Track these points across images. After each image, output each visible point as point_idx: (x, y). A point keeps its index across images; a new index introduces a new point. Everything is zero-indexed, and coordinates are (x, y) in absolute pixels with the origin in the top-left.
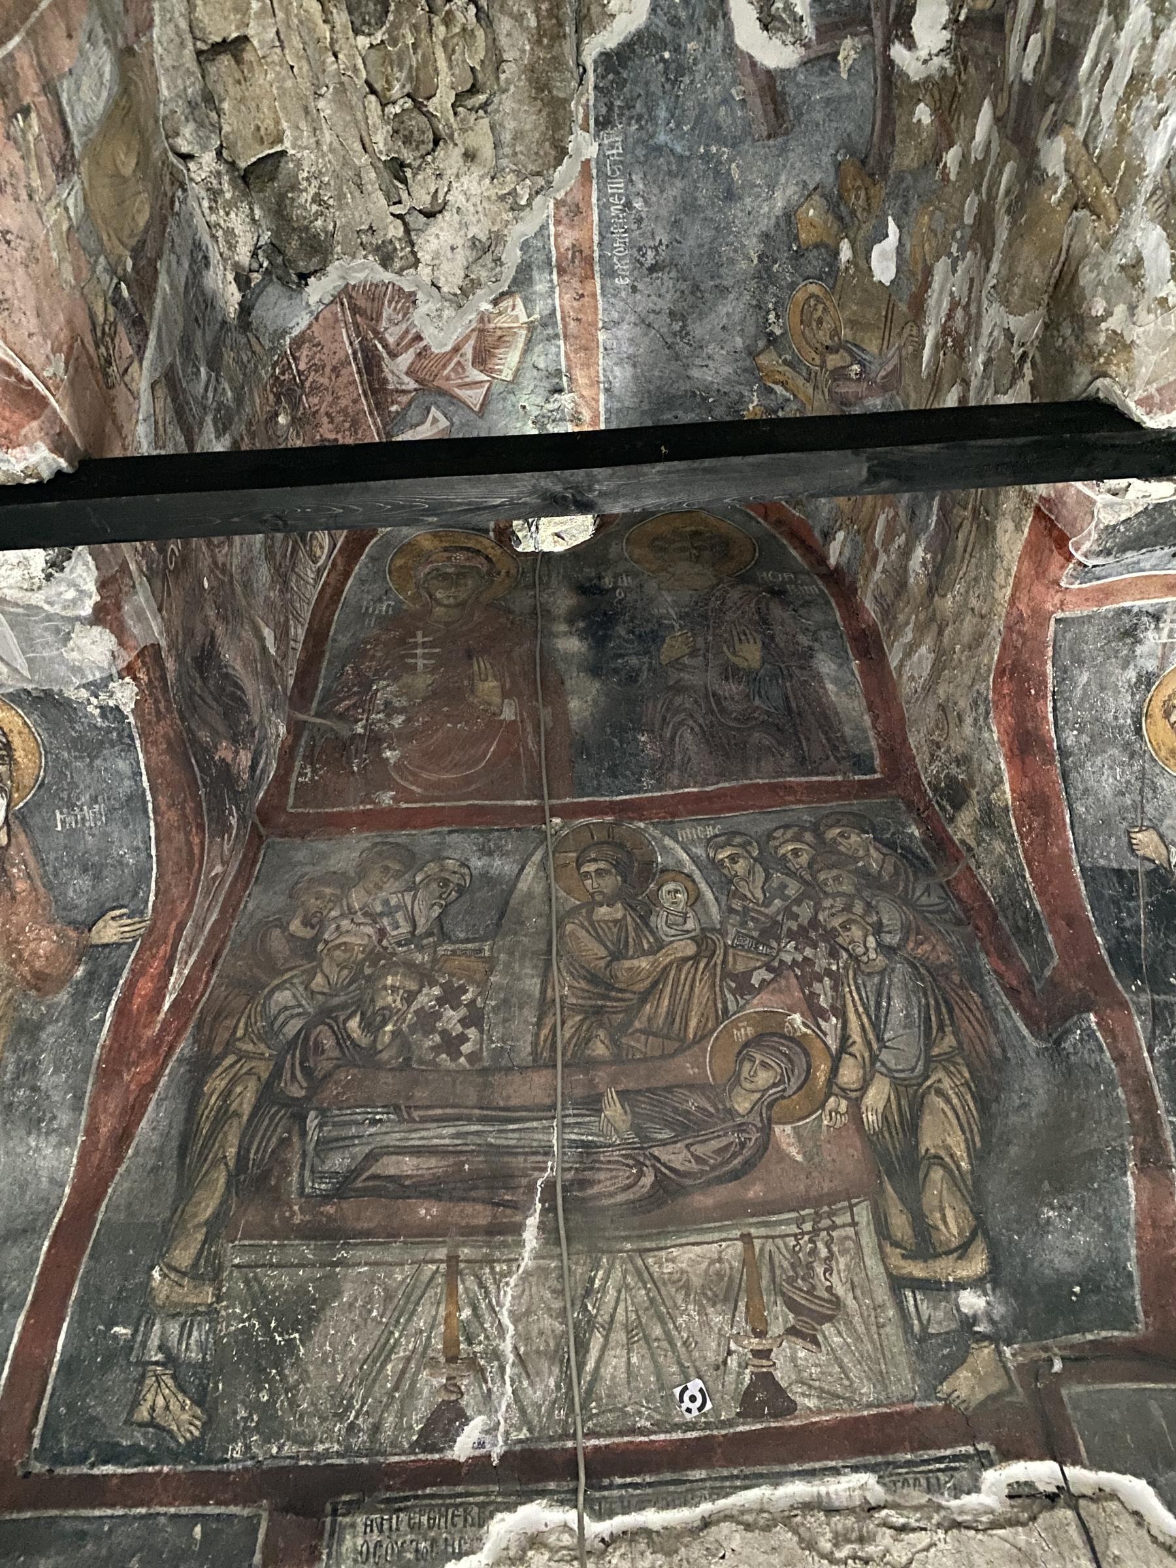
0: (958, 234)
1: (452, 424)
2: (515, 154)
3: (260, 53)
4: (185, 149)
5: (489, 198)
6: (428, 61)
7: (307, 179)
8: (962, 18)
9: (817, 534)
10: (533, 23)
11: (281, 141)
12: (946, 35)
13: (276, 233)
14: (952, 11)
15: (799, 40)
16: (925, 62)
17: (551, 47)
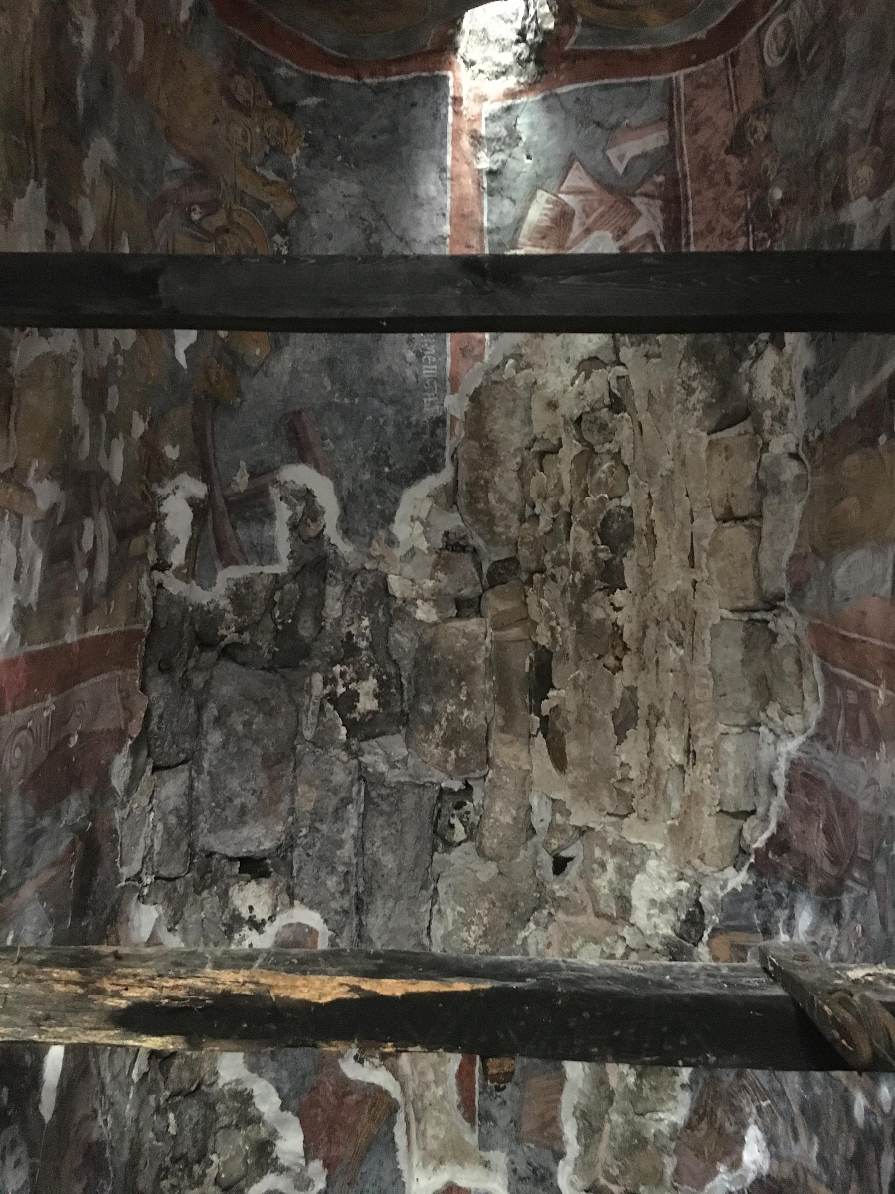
0: (119, 373)
1: (603, 151)
2: (514, 400)
3: (710, 511)
4: (794, 464)
5: (540, 367)
6: (577, 480)
7: (695, 410)
8: (153, 525)
9: (211, 9)
10: (491, 496)
11: (710, 442)
12: (163, 510)
13: (734, 370)
14: (162, 526)
15: (282, 486)
16: (177, 487)
17: (479, 478)
